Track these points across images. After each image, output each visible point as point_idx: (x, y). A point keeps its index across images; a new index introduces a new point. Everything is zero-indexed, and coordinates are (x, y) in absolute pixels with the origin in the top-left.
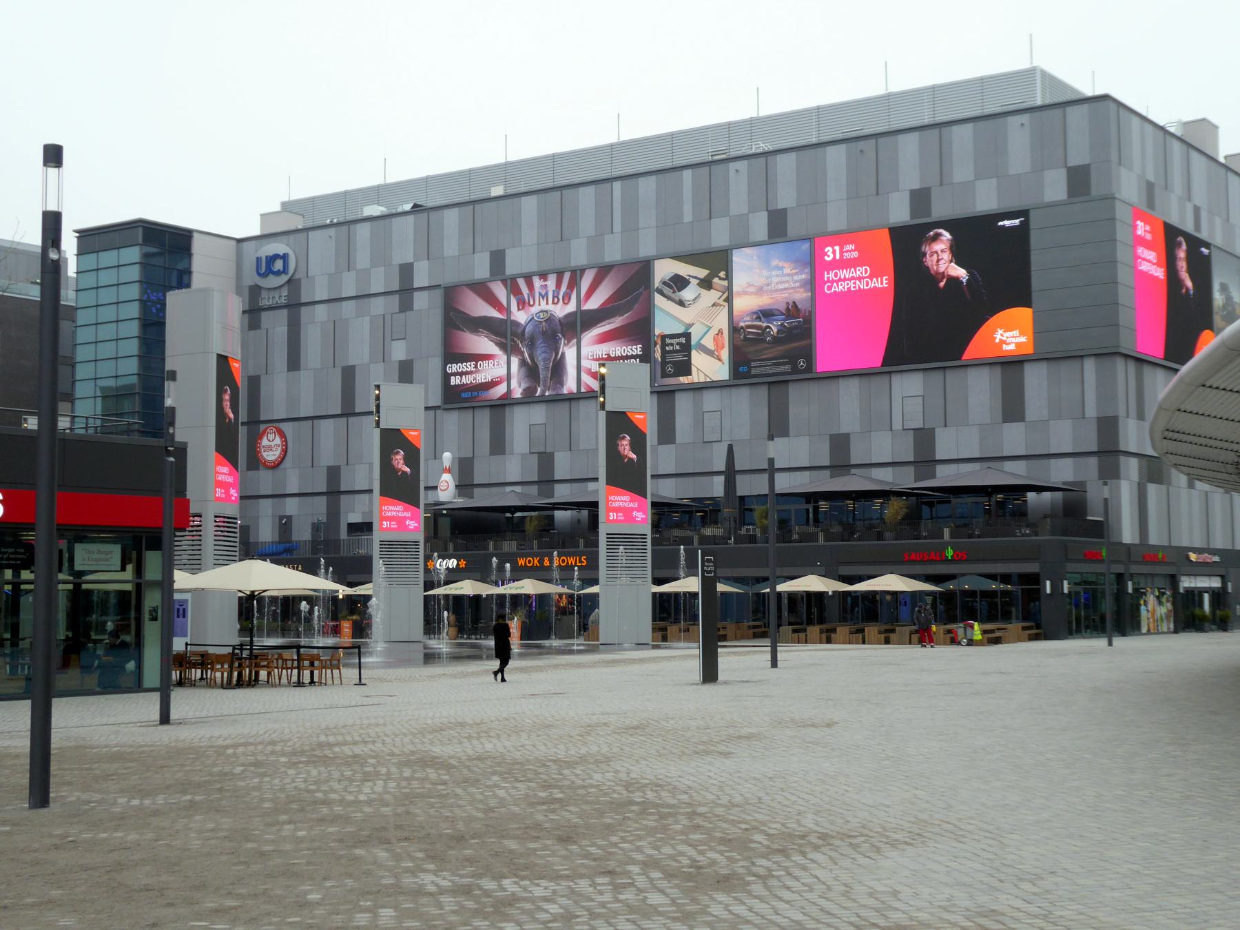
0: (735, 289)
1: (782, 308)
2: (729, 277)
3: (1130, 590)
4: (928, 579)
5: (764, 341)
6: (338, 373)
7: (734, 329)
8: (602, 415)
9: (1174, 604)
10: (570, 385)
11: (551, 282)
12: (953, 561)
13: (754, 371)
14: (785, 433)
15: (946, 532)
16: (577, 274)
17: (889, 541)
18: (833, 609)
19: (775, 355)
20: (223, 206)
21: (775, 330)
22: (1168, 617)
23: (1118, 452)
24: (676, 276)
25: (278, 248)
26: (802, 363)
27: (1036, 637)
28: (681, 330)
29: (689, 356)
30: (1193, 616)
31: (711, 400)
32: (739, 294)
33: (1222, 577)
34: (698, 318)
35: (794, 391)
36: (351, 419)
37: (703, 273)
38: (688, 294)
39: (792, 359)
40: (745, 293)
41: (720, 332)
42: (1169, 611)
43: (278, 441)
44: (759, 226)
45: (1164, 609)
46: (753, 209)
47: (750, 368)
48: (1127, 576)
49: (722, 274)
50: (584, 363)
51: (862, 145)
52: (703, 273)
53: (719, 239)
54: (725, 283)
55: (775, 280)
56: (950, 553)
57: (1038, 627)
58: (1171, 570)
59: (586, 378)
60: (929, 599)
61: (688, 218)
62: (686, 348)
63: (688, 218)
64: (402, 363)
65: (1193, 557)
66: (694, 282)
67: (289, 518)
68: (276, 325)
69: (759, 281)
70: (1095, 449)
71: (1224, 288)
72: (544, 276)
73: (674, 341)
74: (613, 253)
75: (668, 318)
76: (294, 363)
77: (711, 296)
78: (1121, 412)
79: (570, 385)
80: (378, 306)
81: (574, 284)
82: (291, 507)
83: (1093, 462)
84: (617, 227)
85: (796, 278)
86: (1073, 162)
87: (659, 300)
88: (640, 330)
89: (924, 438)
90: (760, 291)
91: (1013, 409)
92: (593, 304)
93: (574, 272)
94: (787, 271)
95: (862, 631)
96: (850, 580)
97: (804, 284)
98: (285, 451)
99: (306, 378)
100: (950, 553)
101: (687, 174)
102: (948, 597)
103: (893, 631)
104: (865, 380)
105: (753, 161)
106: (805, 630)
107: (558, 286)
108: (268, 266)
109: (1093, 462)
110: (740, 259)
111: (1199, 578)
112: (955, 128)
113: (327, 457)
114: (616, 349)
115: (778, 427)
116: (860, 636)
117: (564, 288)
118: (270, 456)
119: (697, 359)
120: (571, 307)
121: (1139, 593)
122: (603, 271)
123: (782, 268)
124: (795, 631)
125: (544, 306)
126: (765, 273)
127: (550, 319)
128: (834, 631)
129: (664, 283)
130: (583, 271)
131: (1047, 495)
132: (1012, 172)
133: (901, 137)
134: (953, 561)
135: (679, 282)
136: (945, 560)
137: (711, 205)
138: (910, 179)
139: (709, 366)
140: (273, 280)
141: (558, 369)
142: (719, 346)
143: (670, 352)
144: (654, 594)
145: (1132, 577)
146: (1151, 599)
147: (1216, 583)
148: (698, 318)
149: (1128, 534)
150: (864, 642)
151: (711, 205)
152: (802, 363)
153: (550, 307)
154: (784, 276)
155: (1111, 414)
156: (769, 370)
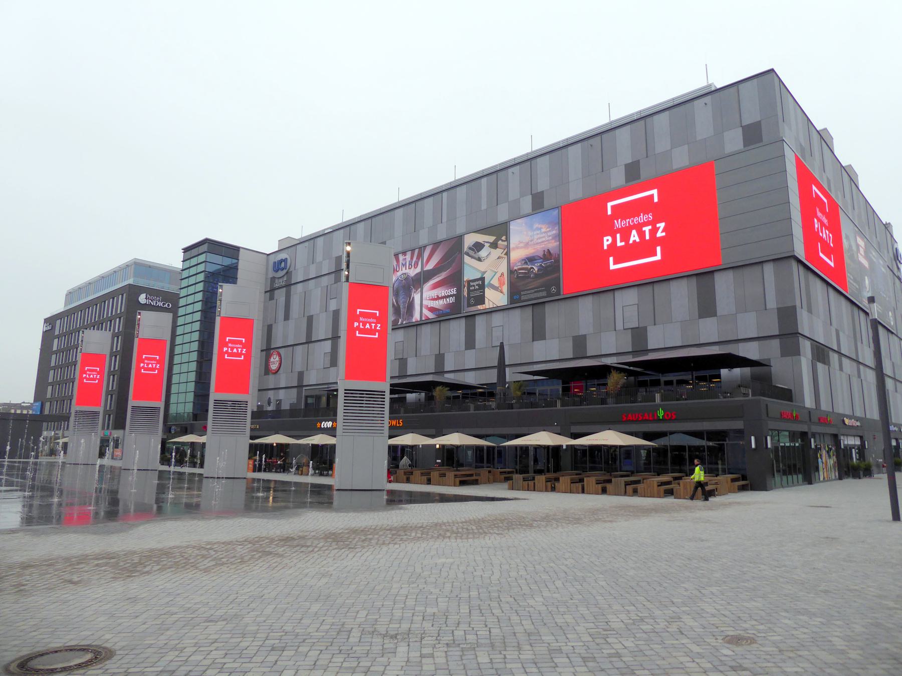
0: (512, 246)
1: (541, 254)
2: (508, 240)
3: (813, 446)
4: (647, 436)
5: (529, 277)
6: (305, 319)
7: (511, 272)
8: (346, 286)
9: (837, 457)
10: (416, 316)
11: (408, 256)
12: (664, 420)
13: (523, 298)
14: (543, 337)
15: (658, 396)
16: (422, 249)
17: (611, 404)
18: (566, 460)
19: (537, 288)
20: (258, 234)
21: (536, 269)
22: (834, 466)
23: (796, 334)
24: (477, 243)
25: (283, 256)
26: (554, 290)
27: (743, 488)
28: (479, 276)
29: (484, 292)
30: (848, 466)
31: (497, 319)
32: (514, 249)
33: (861, 437)
34: (490, 268)
35: (548, 308)
36: (310, 345)
37: (492, 239)
38: (483, 253)
39: (547, 287)
40: (517, 248)
41: (502, 274)
42: (835, 463)
43: (277, 359)
44: (527, 204)
45: (832, 461)
46: (523, 195)
47: (520, 296)
48: (810, 435)
49: (504, 238)
50: (425, 302)
51: (591, 141)
52: (492, 239)
53: (502, 217)
54: (505, 243)
55: (536, 237)
56: (661, 413)
57: (744, 478)
58: (833, 431)
59: (425, 312)
60: (643, 453)
61: (484, 207)
62: (482, 287)
63: (484, 207)
64: (334, 311)
65: (847, 421)
66: (487, 245)
67: (280, 400)
68: (280, 295)
69: (526, 239)
70: (777, 333)
71: (847, 238)
72: (404, 253)
73: (475, 284)
74: (442, 235)
75: (472, 269)
76: (287, 317)
77: (498, 252)
78: (798, 304)
79: (416, 316)
80: (325, 281)
81: (420, 255)
82: (282, 394)
83: (776, 343)
84: (445, 219)
85: (550, 234)
86: (746, 122)
87: (467, 259)
88: (455, 280)
89: (639, 334)
90: (527, 245)
91: (707, 307)
92: (430, 266)
93: (420, 248)
94: (543, 230)
95: (581, 480)
96: (576, 436)
97: (554, 237)
98: (280, 364)
99: (291, 323)
100: (661, 413)
101: (484, 180)
102: (661, 452)
103: (610, 481)
104: (596, 297)
105: (522, 165)
106: (534, 479)
107: (412, 258)
108: (279, 265)
109: (776, 343)
110: (514, 227)
111: (849, 438)
112: (656, 117)
113: (298, 368)
114: (442, 292)
115: (539, 333)
116: (580, 485)
117: (415, 259)
118: (274, 367)
119: (489, 293)
120: (418, 270)
121: (818, 449)
122: (436, 245)
123: (540, 229)
124: (524, 479)
125: (404, 271)
126: (530, 233)
127: (407, 278)
128: (557, 479)
129: (470, 248)
130: (425, 247)
131: (737, 371)
132: (699, 138)
133: (618, 131)
134: (664, 420)
135: (478, 246)
136: (658, 420)
137: (497, 197)
138: (625, 157)
139: (496, 298)
140: (280, 272)
141: (410, 307)
142: (502, 284)
143: (473, 290)
144: (390, 447)
145: (814, 435)
146: (824, 453)
147: (858, 442)
148: (490, 268)
149: (809, 403)
150: (583, 492)
151: (497, 197)
152: (554, 290)
153: (408, 271)
154: (542, 233)
155: (789, 304)
156: (533, 296)
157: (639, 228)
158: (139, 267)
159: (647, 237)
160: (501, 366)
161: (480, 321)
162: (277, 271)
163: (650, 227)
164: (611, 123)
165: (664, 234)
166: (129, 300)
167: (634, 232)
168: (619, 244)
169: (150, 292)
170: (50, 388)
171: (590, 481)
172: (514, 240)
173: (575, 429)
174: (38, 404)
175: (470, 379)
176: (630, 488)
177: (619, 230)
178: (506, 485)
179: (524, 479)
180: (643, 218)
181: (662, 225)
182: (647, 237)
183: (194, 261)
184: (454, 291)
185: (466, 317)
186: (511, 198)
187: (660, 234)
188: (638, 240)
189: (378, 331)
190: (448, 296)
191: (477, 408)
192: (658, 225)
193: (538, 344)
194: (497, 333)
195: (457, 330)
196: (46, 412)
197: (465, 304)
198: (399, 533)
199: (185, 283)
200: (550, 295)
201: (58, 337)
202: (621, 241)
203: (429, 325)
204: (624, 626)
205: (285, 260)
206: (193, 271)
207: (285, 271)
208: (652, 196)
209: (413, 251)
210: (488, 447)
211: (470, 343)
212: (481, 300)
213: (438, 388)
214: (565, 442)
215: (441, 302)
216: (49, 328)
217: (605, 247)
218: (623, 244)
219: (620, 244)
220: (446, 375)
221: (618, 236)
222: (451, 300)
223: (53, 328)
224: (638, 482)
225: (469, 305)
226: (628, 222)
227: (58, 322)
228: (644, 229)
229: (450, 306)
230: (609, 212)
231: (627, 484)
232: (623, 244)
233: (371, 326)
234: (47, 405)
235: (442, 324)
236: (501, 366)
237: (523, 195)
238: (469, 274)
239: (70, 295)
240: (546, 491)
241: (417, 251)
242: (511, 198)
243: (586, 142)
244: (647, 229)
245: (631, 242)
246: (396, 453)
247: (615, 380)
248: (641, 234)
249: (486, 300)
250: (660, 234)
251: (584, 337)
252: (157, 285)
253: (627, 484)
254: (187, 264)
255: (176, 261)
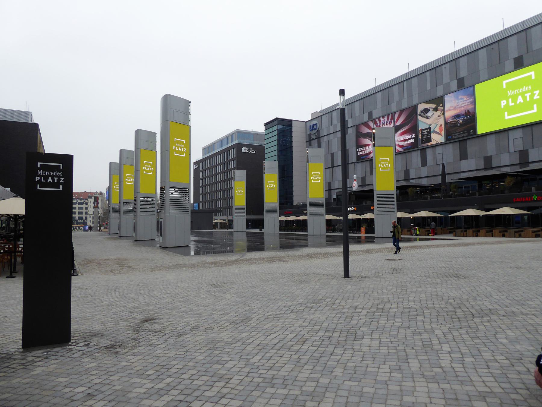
0: (446, 109)
1: (464, 113)
2: (444, 106)
4: (528, 209)
5: (457, 126)
6: (330, 155)
7: (446, 124)
11: (386, 119)
13: (454, 137)
15: (534, 189)
16: (393, 114)
20: (301, 113)
25: (314, 122)
26: (472, 132)
28: (427, 127)
31: (439, 150)
32: (447, 111)
35: (469, 143)
37: (434, 106)
38: (429, 114)
40: (450, 110)
41: (441, 125)
44: (454, 85)
46: (451, 80)
47: (452, 136)
49: (441, 105)
50: (397, 143)
52: (434, 106)
53: (440, 93)
54: (442, 108)
55: (460, 103)
56: (535, 197)
59: (397, 148)
60: (526, 217)
61: (429, 88)
62: (430, 133)
63: (429, 88)
66: (431, 110)
69: (454, 104)
72: (383, 117)
73: (425, 131)
74: (405, 105)
75: (423, 123)
77: (438, 113)
81: (393, 118)
87: (420, 118)
88: (414, 129)
89: (524, 154)
90: (455, 108)
92: (399, 123)
93: (392, 114)
94: (465, 99)
96: (488, 210)
101: (428, 73)
103: (506, 231)
107: (388, 119)
108: (312, 128)
110: (447, 98)
112: (533, 29)
114: (406, 137)
115: (463, 156)
116: (491, 233)
117: (390, 120)
119: (433, 136)
122: (401, 112)
123: (463, 98)
124: (461, 232)
126: (457, 101)
128: (479, 231)
129: (421, 112)
130: (395, 113)
134: (537, 200)
135: (426, 111)
136: (534, 201)
137: (436, 82)
139: (437, 138)
142: (441, 130)
150: (492, 236)
151: (436, 82)
152: (472, 132)
156: (459, 136)
157: (523, 94)
158: (240, 134)
159: (528, 100)
160: (444, 175)
161: (429, 152)
162: (311, 130)
163: (530, 94)
164: (505, 30)
165: (538, 97)
166: (237, 151)
167: (520, 97)
168: (511, 104)
169: (247, 146)
170: (201, 196)
171: (496, 231)
172: (447, 106)
173: (487, 207)
174: (196, 204)
175: (425, 182)
176: (517, 234)
177: (510, 97)
178: (452, 235)
179: (461, 232)
180: (525, 89)
181: (537, 92)
182: (528, 100)
183: (271, 130)
184: (413, 136)
185: (421, 149)
186: (444, 82)
187: (536, 97)
188: (522, 101)
189: (61, 184)
190: (410, 139)
191: (432, 198)
192: (535, 92)
193: (463, 162)
194: (439, 157)
195: (416, 156)
196: (201, 208)
197: (421, 142)
198: (429, 247)
199: (267, 141)
200: (469, 135)
201: (202, 171)
202: (512, 103)
203: (400, 155)
204: (526, 370)
205: (316, 125)
206: (271, 135)
207: (316, 130)
208: (531, 75)
209: (388, 115)
210: (439, 217)
211: (424, 163)
212: (429, 140)
213: (410, 189)
214: (482, 213)
215: (406, 142)
216: (197, 167)
217: (503, 107)
218: (513, 104)
219: (511, 104)
220: (411, 181)
221: (510, 99)
222: (412, 141)
223: (199, 167)
224: (522, 231)
225: (422, 143)
226: (516, 91)
227: (201, 164)
228: (526, 95)
229: (411, 144)
230: (505, 87)
231: (515, 232)
232: (513, 104)
233: (53, 180)
234: (201, 204)
235: (407, 154)
236: (444, 175)
237: (451, 80)
238: (421, 126)
239: (205, 150)
240: (473, 236)
241: (390, 115)
242: (445, 81)
243: (489, 47)
244: (528, 95)
245: (518, 103)
246: (328, 222)
247: (508, 182)
248: (524, 98)
249: (432, 140)
250: (536, 97)
251: (491, 157)
252: (249, 142)
253: (515, 232)
254: (267, 131)
255: (261, 129)
